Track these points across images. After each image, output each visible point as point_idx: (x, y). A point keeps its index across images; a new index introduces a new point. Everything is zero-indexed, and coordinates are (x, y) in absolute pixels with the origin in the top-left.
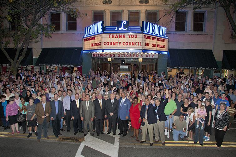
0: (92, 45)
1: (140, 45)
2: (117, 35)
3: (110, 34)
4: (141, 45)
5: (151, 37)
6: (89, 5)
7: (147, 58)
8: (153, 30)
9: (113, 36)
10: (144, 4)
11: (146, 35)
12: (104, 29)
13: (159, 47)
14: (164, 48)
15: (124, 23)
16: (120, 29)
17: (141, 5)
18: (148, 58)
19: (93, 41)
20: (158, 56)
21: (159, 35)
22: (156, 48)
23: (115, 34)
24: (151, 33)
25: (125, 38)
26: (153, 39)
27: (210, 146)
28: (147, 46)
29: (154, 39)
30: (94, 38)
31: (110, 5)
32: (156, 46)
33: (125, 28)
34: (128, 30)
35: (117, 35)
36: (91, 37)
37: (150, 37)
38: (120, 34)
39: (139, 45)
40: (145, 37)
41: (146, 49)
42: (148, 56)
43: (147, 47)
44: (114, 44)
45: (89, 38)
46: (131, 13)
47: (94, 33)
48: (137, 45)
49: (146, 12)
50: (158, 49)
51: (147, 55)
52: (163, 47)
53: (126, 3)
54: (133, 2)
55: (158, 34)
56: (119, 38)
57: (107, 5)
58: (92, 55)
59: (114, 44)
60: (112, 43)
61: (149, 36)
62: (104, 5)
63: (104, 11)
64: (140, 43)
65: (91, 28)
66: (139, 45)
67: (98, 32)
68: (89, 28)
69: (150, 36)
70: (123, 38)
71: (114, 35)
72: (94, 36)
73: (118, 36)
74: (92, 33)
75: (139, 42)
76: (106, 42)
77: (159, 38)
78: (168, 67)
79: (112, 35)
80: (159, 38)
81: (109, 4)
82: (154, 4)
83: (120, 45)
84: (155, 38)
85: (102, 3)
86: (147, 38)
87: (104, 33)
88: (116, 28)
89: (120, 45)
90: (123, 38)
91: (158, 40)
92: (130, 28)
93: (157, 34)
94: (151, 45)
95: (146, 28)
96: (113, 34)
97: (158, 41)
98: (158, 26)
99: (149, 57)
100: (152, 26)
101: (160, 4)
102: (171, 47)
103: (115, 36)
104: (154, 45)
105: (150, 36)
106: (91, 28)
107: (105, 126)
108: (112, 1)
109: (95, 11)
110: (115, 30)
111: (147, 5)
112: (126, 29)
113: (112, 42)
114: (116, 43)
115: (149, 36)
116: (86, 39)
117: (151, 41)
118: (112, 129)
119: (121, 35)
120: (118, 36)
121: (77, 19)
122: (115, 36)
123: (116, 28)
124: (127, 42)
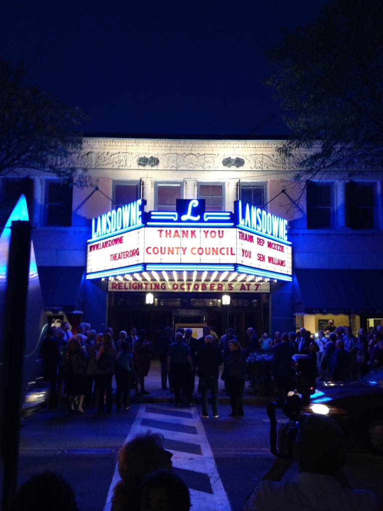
0: (114, 257)
1: (232, 254)
2: (176, 231)
3: (160, 229)
4: (234, 254)
5: (254, 238)
6: (105, 167)
7: (244, 291)
8: (258, 223)
9: (168, 234)
10: (234, 168)
11: (243, 232)
12: (146, 218)
13: (273, 263)
14: (281, 267)
15: (194, 204)
16: (184, 218)
17: (226, 168)
18: (247, 291)
19: (117, 249)
20: (268, 287)
21: (272, 234)
22: (266, 265)
23: (173, 230)
24: (254, 229)
25: (195, 237)
26: (258, 242)
28: (247, 257)
29: (260, 242)
30: (120, 240)
31: (155, 168)
32: (267, 259)
34: (201, 220)
35: (176, 231)
36: (111, 239)
37: (252, 237)
38: (185, 229)
39: (228, 254)
40: (242, 237)
41: (243, 264)
42: (246, 287)
43: (247, 261)
44: (171, 251)
45: (106, 243)
46: (204, 188)
48: (224, 254)
49: (237, 186)
50: (271, 267)
51: (243, 285)
52: (282, 263)
53: (191, 165)
54: (208, 162)
56: (183, 237)
57: (148, 167)
58: (110, 286)
59: (171, 251)
60: (167, 250)
61: (250, 234)
62: (141, 167)
63: (141, 183)
64: (231, 248)
65: (110, 218)
66: (228, 254)
67: (130, 225)
68: (105, 218)
69: (252, 235)
70: (192, 237)
71: (170, 231)
72: (119, 236)
73: (180, 234)
75: (228, 248)
76: (150, 248)
77: (272, 242)
79: (166, 231)
80: (272, 242)
81: (152, 166)
82: (255, 166)
83: (184, 254)
84: (263, 240)
85: (137, 164)
86: (246, 239)
87: (146, 226)
88: (174, 216)
89: (184, 254)
90: (192, 237)
91: (270, 245)
92: (207, 216)
93: (267, 233)
94: (254, 257)
95: (244, 217)
96: (168, 229)
97: (271, 248)
99: (248, 289)
100: (255, 212)
101: (269, 167)
102: (299, 265)
103: (173, 233)
104: (261, 258)
105: (252, 235)
106: (110, 218)
108: (159, 159)
109: (118, 181)
110: (172, 221)
111: (241, 168)
113: (165, 248)
114: (175, 250)
115: (250, 234)
116: (97, 246)
117: (253, 247)
119: (187, 231)
120: (180, 234)
122: (173, 233)
123: (174, 216)
124: (200, 248)
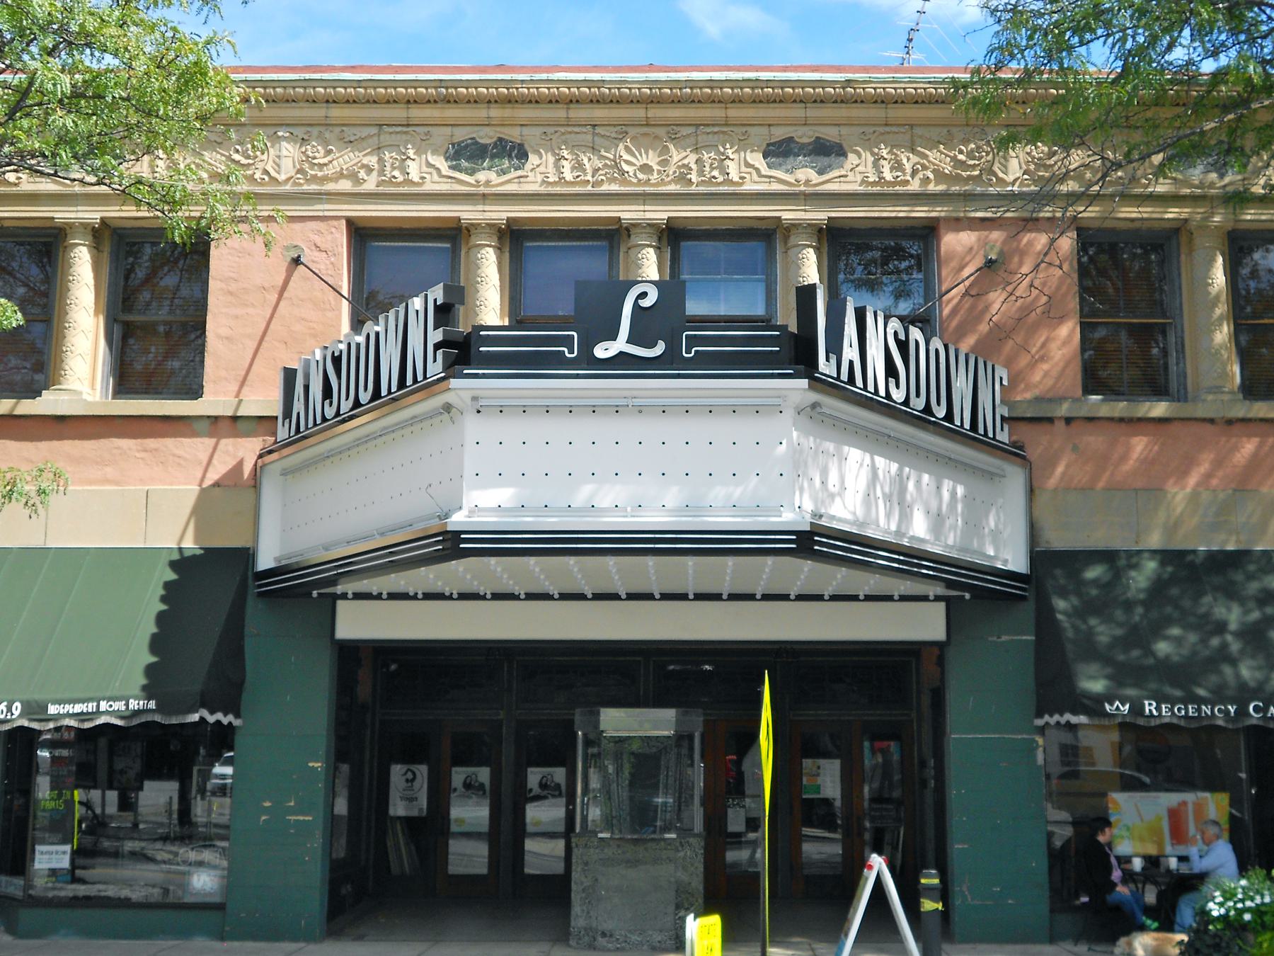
8: (891, 371)
15: (643, 295)
16: (602, 351)
27: (690, 519)
33: (651, 345)
47: (364, 397)
55: (941, 412)
74: (346, 406)
78: (1039, 714)
92: (693, 341)
95: (835, 347)
98: (937, 343)
107: (812, 288)
112: (659, 349)
118: (778, 333)
121: (220, 259)
